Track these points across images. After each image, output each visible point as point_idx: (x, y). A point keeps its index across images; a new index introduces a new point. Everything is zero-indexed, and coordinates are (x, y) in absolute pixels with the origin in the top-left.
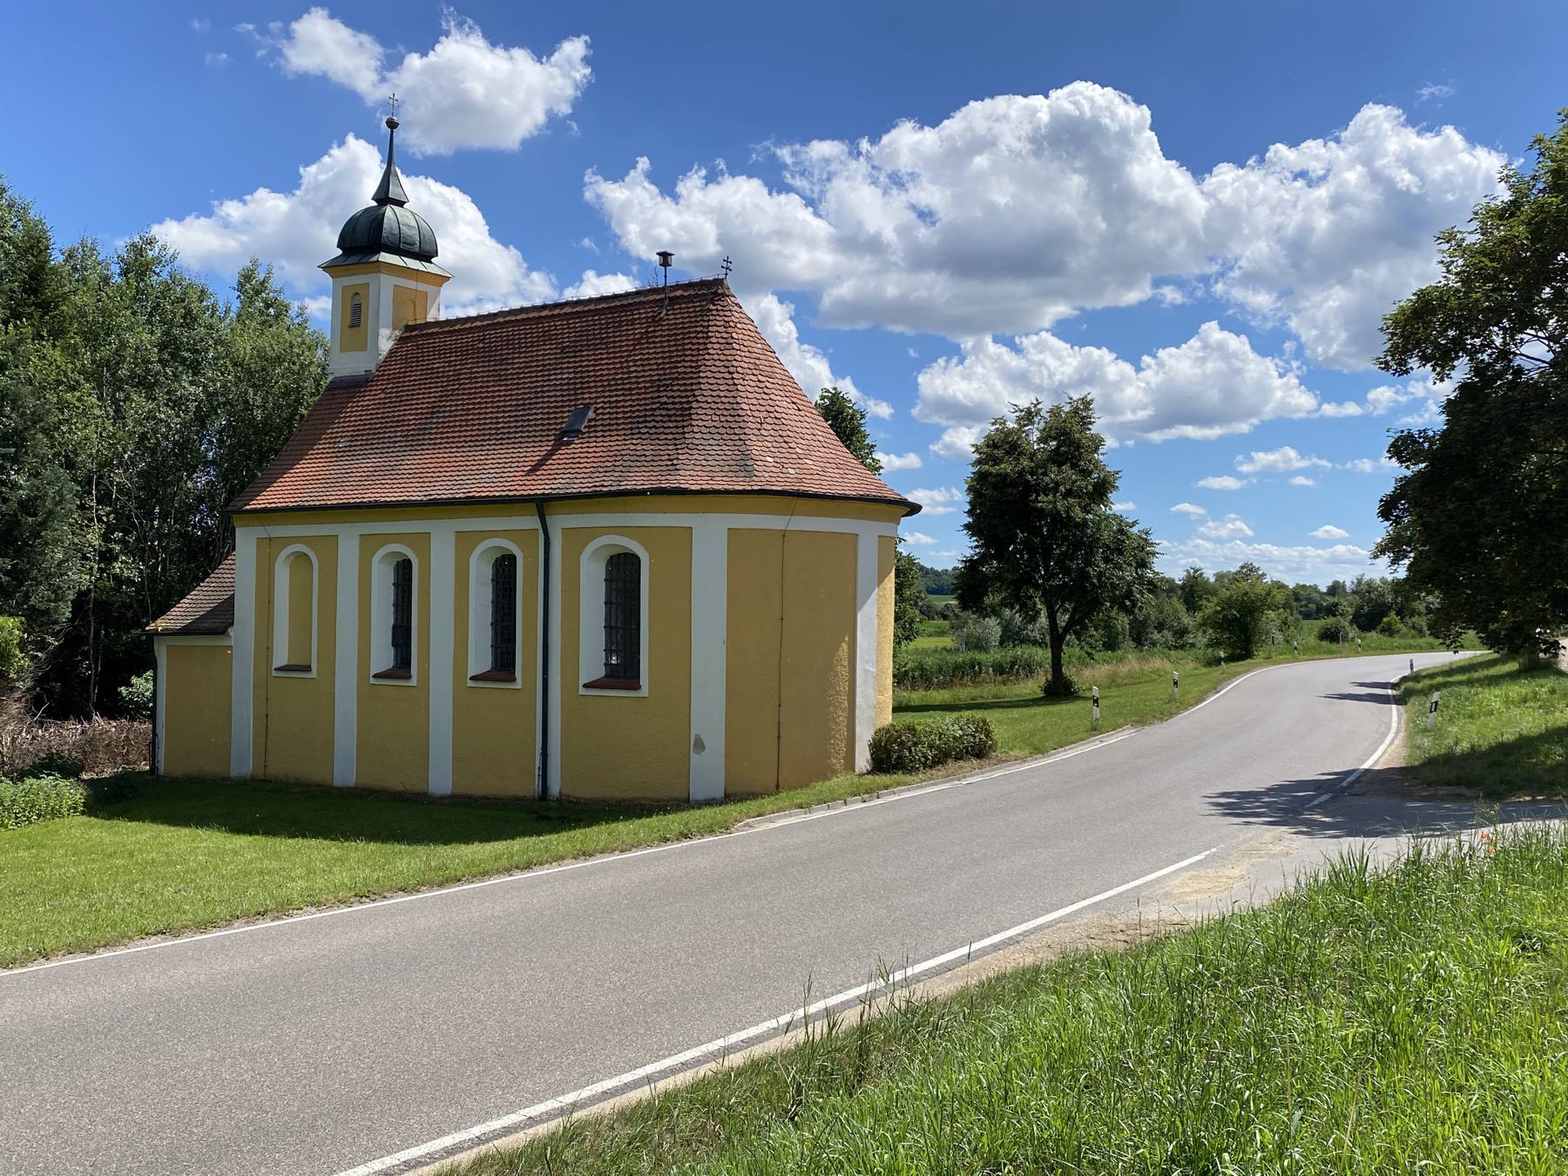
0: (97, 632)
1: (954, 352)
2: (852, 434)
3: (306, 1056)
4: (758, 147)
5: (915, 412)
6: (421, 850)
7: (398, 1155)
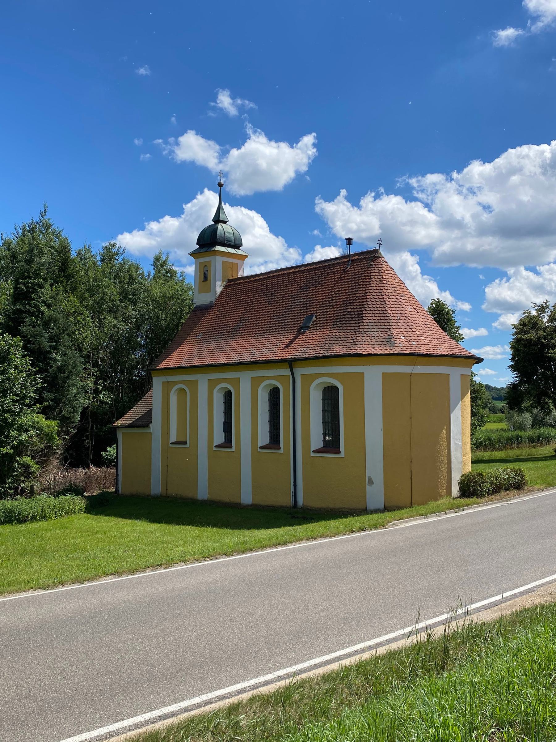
0: (92, 426)
1: (503, 275)
2: (448, 322)
3: (175, 639)
4: (400, 180)
5: (483, 307)
6: (237, 532)
7: (214, 693)
